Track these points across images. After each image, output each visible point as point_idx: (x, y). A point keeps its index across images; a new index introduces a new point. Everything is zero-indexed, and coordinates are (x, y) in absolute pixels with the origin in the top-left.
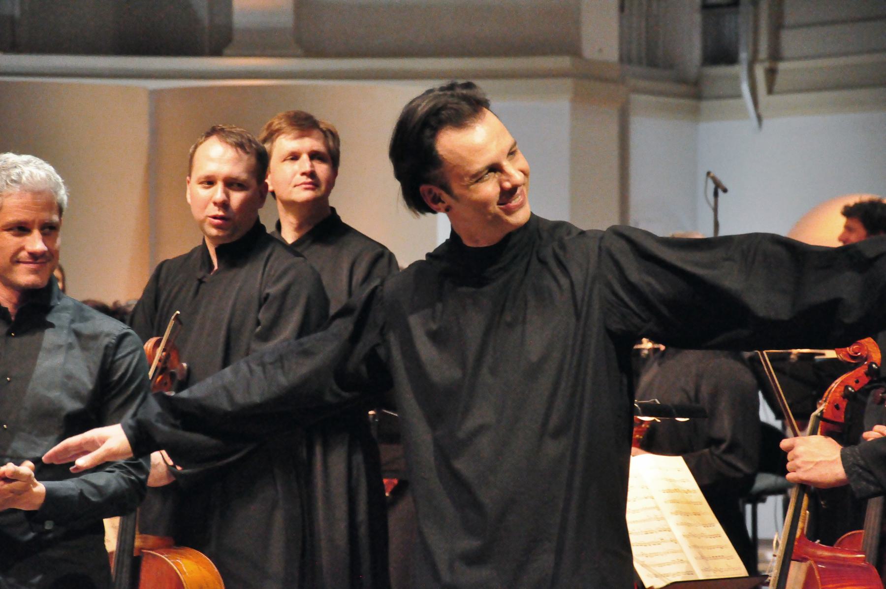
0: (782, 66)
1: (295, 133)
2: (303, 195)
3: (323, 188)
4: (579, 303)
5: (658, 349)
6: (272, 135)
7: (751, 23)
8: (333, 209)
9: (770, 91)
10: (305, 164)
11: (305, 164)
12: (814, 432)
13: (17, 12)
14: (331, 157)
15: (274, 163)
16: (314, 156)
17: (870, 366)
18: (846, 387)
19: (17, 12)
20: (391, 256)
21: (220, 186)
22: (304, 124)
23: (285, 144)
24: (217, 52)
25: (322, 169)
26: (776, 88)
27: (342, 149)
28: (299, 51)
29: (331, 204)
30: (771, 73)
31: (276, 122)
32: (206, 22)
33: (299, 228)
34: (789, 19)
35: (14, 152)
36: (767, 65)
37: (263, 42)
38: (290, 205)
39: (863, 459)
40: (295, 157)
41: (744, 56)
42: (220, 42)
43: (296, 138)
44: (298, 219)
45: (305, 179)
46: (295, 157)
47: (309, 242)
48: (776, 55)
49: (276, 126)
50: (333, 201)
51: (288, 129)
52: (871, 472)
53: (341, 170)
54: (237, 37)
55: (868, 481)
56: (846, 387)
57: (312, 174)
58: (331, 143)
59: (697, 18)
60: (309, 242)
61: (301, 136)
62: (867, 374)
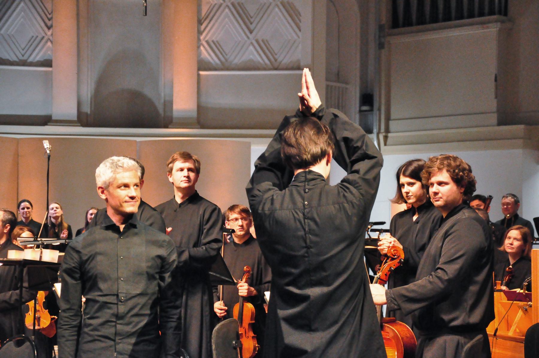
0: (389, 135)
1: (182, 160)
2: (184, 185)
3: (192, 182)
4: (304, 225)
5: (54, 318)
6: (173, 161)
7: (378, 118)
8: (196, 191)
9: (385, 145)
10: (185, 173)
11: (185, 173)
12: (376, 283)
13: (89, 112)
14: (196, 170)
15: (174, 171)
16: (189, 170)
17: (400, 260)
18: (391, 268)
19: (89, 112)
20: (219, 209)
21: (186, 170)
22: (187, 157)
23: (179, 164)
24: (166, 127)
25: (192, 175)
26: (388, 143)
27: (201, 167)
28: (199, 126)
29: (196, 189)
30: (386, 138)
31: (176, 155)
32: (163, 115)
33: (182, 198)
34: (392, 117)
35: (116, 156)
36: (384, 134)
37: (184, 123)
38: (179, 188)
39: (394, 295)
40: (182, 170)
41: (375, 131)
42: (166, 122)
43: (183, 163)
44: (183, 193)
45: (185, 179)
46: (182, 170)
47: (187, 203)
48: (387, 131)
49: (175, 158)
50: (197, 187)
51: (180, 159)
52: (396, 300)
53: (200, 175)
54: (174, 121)
55: (395, 304)
56: (391, 268)
57: (188, 177)
58: (197, 165)
59: (357, 116)
60: (187, 203)
61: (185, 162)
62: (398, 263)
